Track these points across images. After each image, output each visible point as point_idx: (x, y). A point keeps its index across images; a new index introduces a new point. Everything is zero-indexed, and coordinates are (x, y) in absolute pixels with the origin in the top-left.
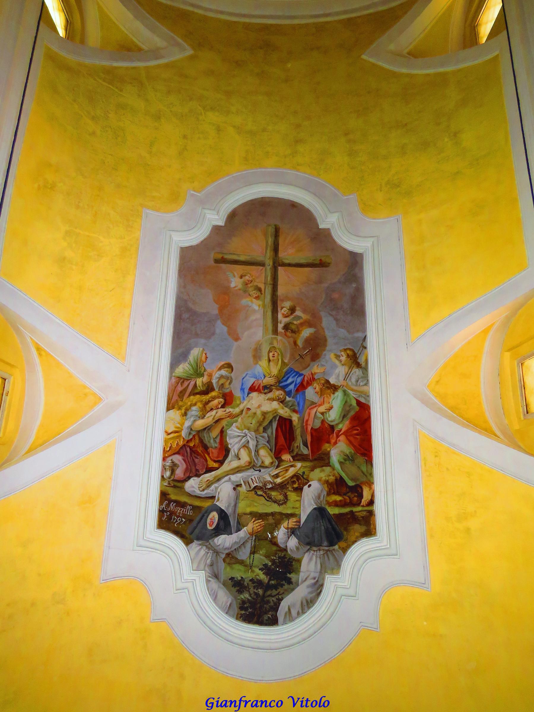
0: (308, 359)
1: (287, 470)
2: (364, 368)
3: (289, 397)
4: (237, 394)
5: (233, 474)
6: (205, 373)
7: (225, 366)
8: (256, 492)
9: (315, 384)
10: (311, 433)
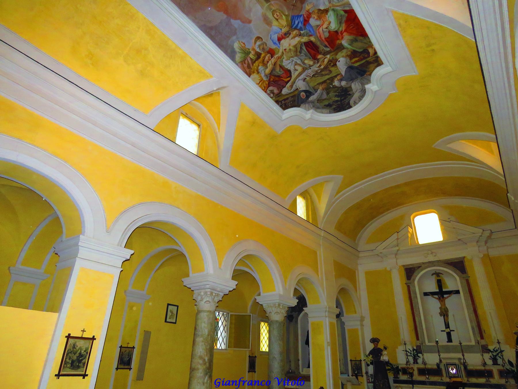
1: (324, 61)
4: (273, 47)
6: (250, 50)
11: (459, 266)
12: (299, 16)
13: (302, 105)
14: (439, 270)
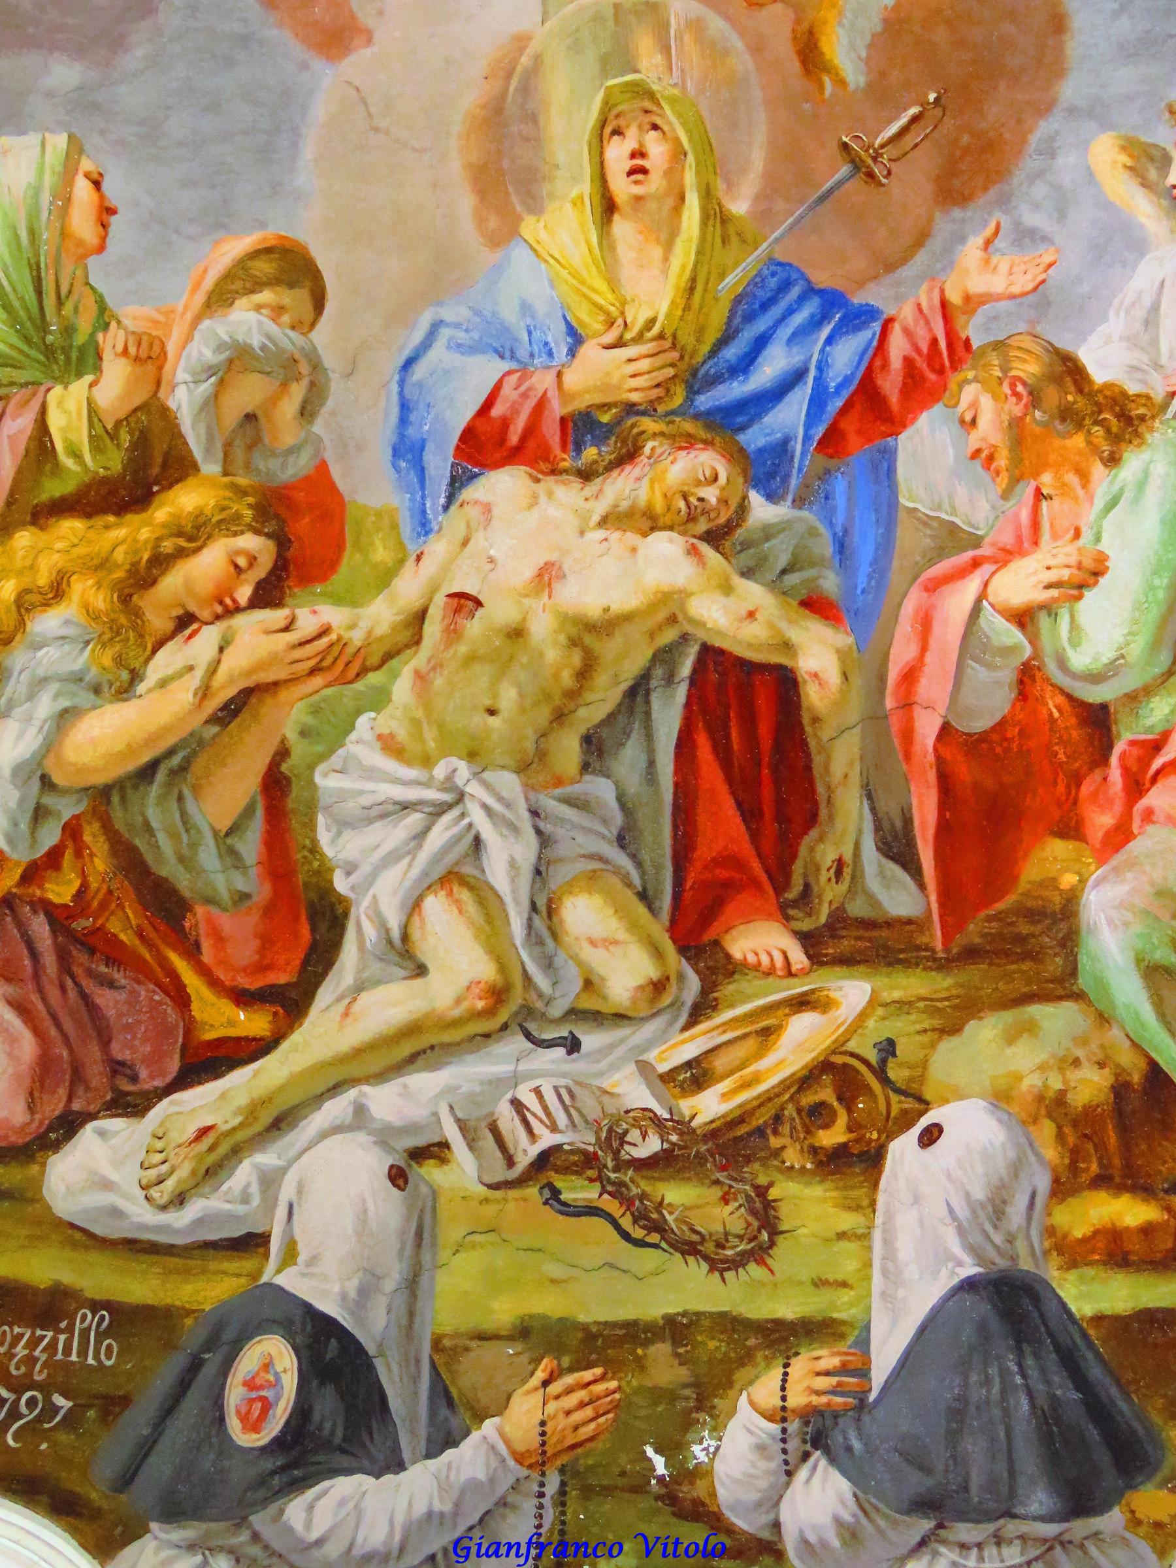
0: (911, 183)
3: (772, 497)
4: (371, 488)
5: (380, 1077)
6: (112, 341)
7: (264, 267)
8: (556, 1193)
9: (969, 393)
10: (940, 761)
12: (839, 310)
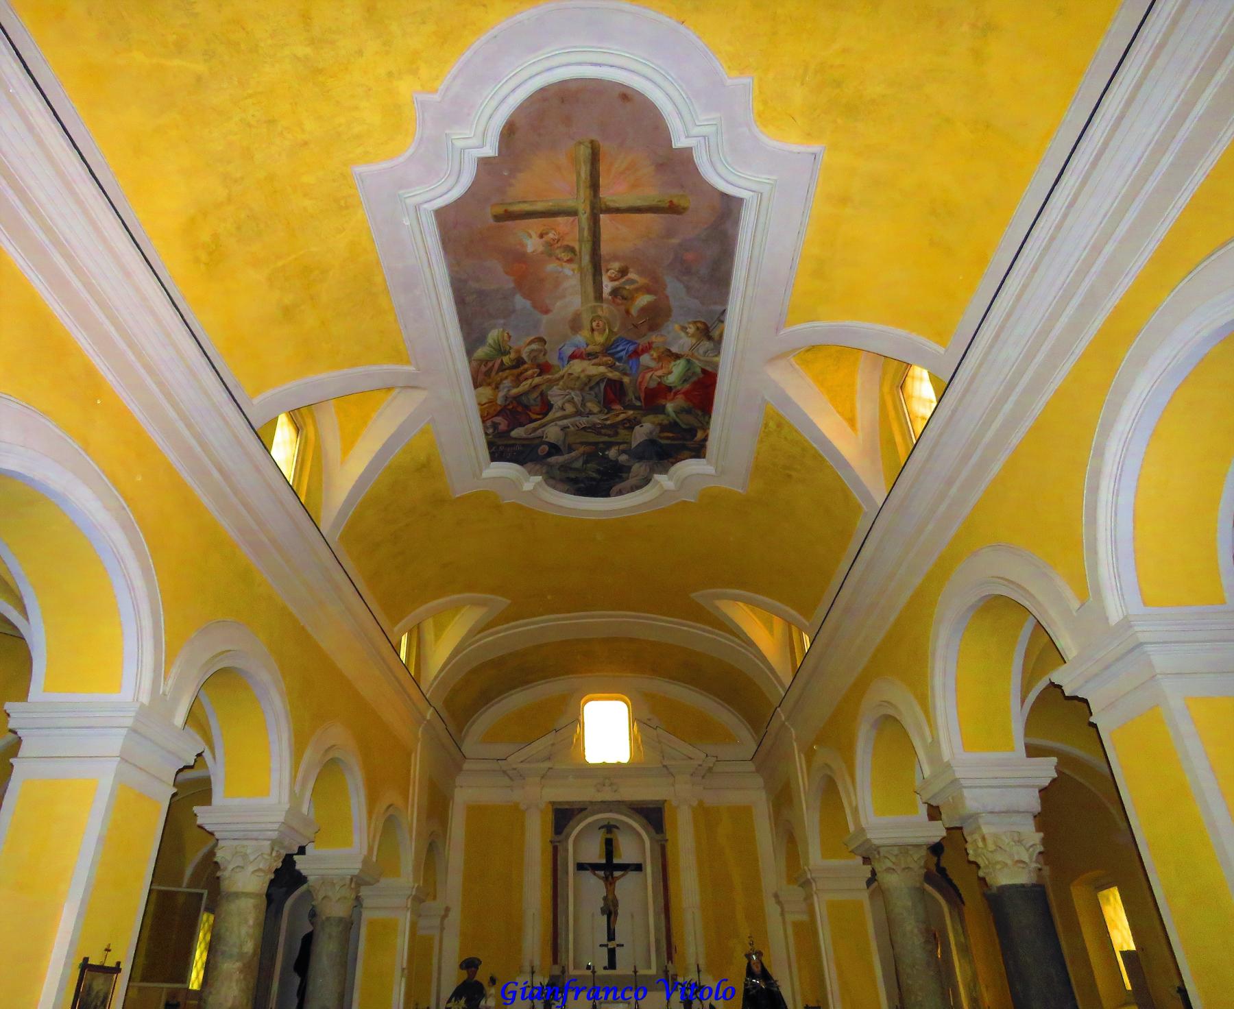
2: (718, 342)
11: (653, 816)
13: (529, 464)
14: (617, 820)
